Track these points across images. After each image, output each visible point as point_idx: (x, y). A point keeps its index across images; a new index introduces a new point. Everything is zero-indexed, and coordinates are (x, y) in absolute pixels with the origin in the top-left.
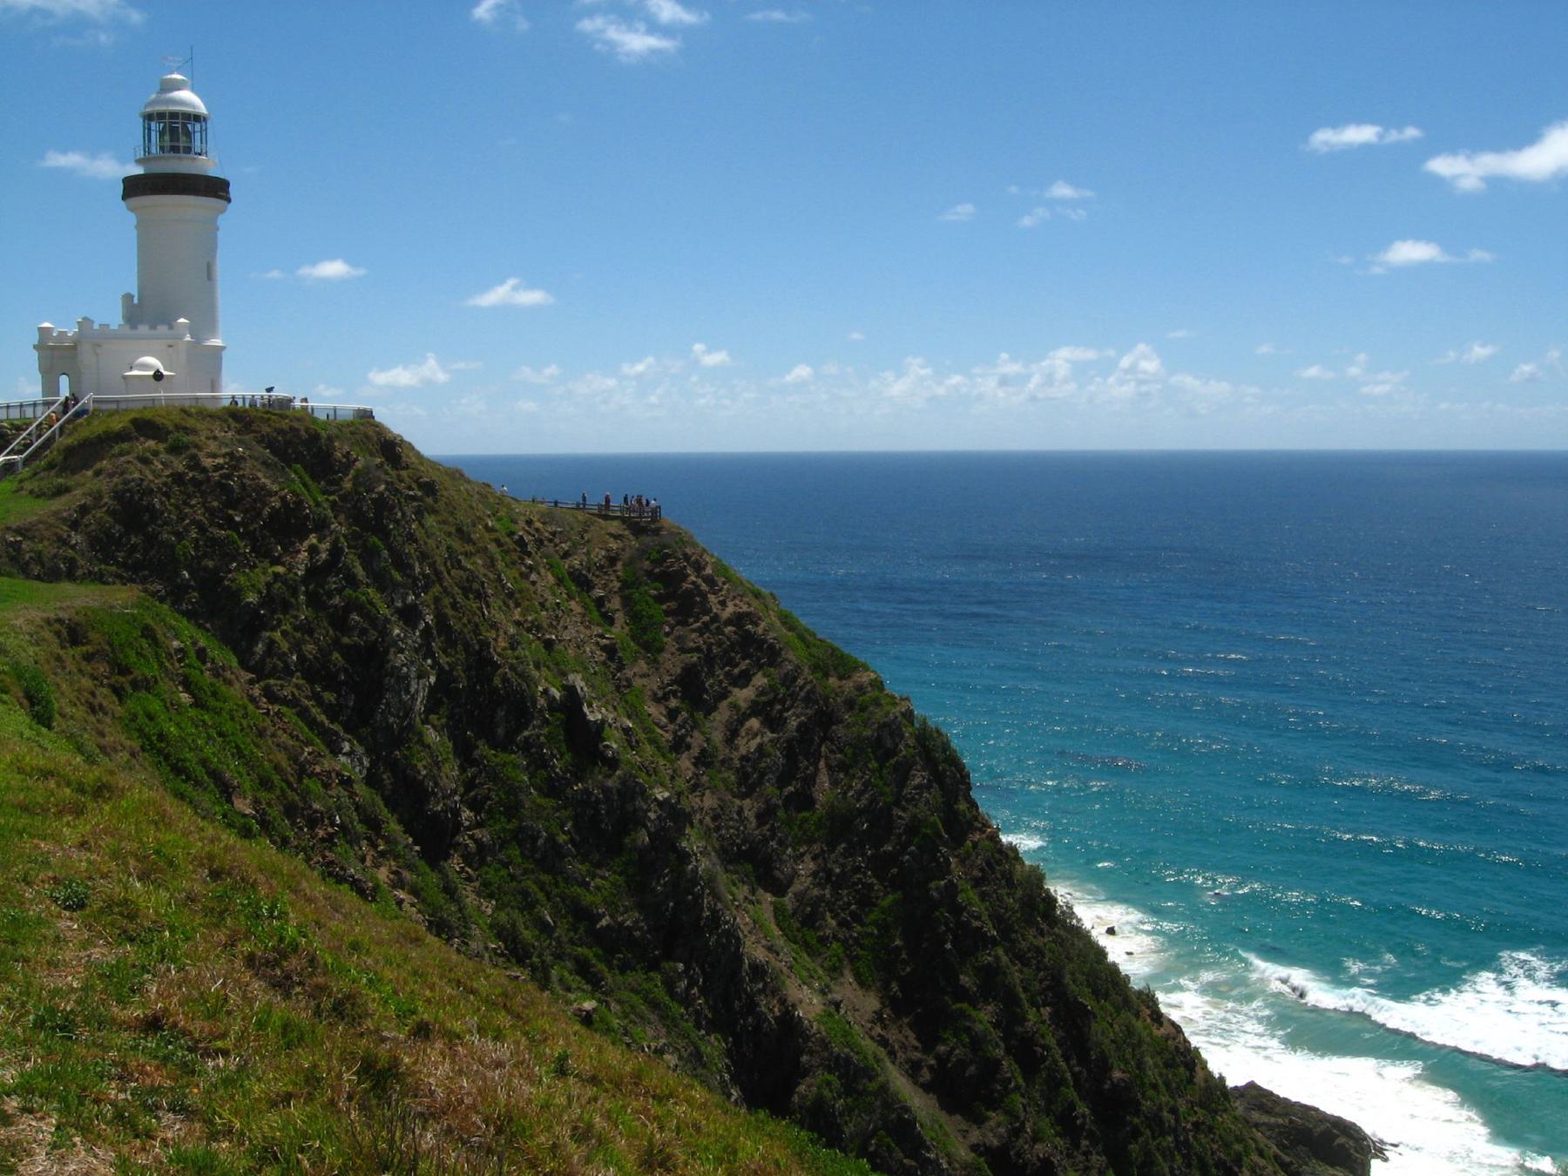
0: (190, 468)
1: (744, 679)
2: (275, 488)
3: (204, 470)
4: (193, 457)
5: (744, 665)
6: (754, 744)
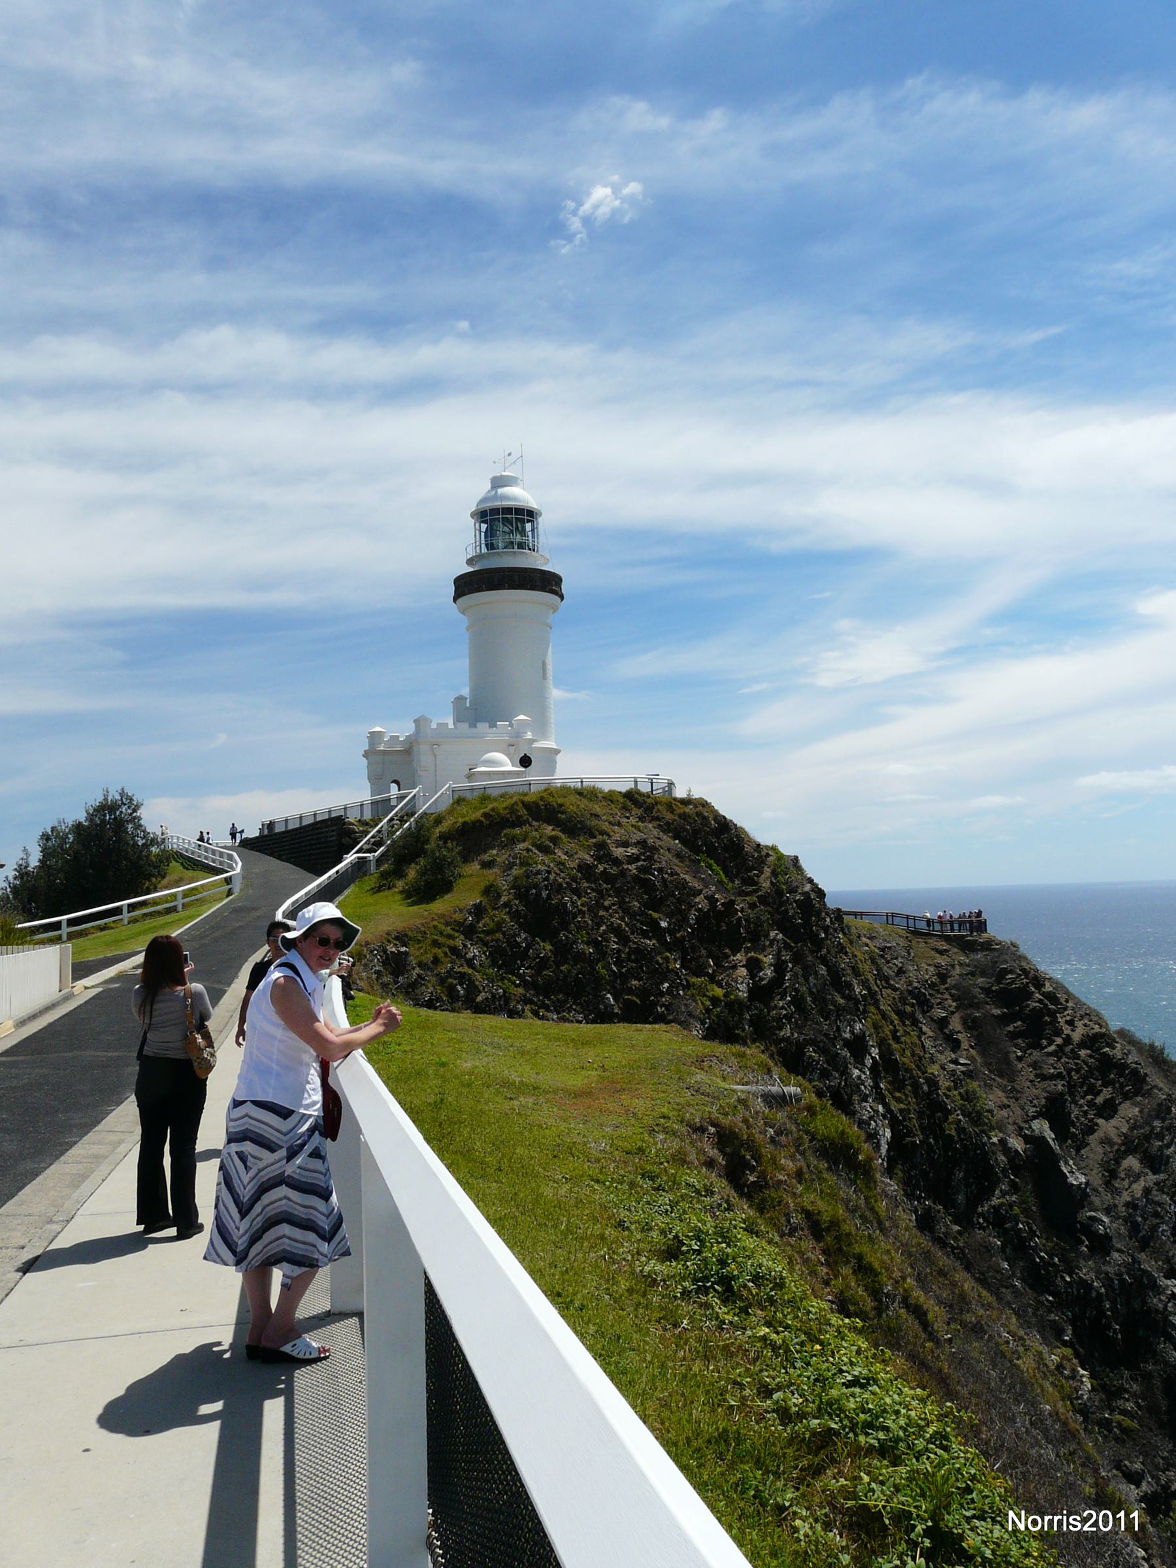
0: (599, 859)
1: (1108, 1110)
2: (697, 885)
3: (616, 862)
4: (602, 846)
5: (1106, 1093)
6: (1138, 1188)
